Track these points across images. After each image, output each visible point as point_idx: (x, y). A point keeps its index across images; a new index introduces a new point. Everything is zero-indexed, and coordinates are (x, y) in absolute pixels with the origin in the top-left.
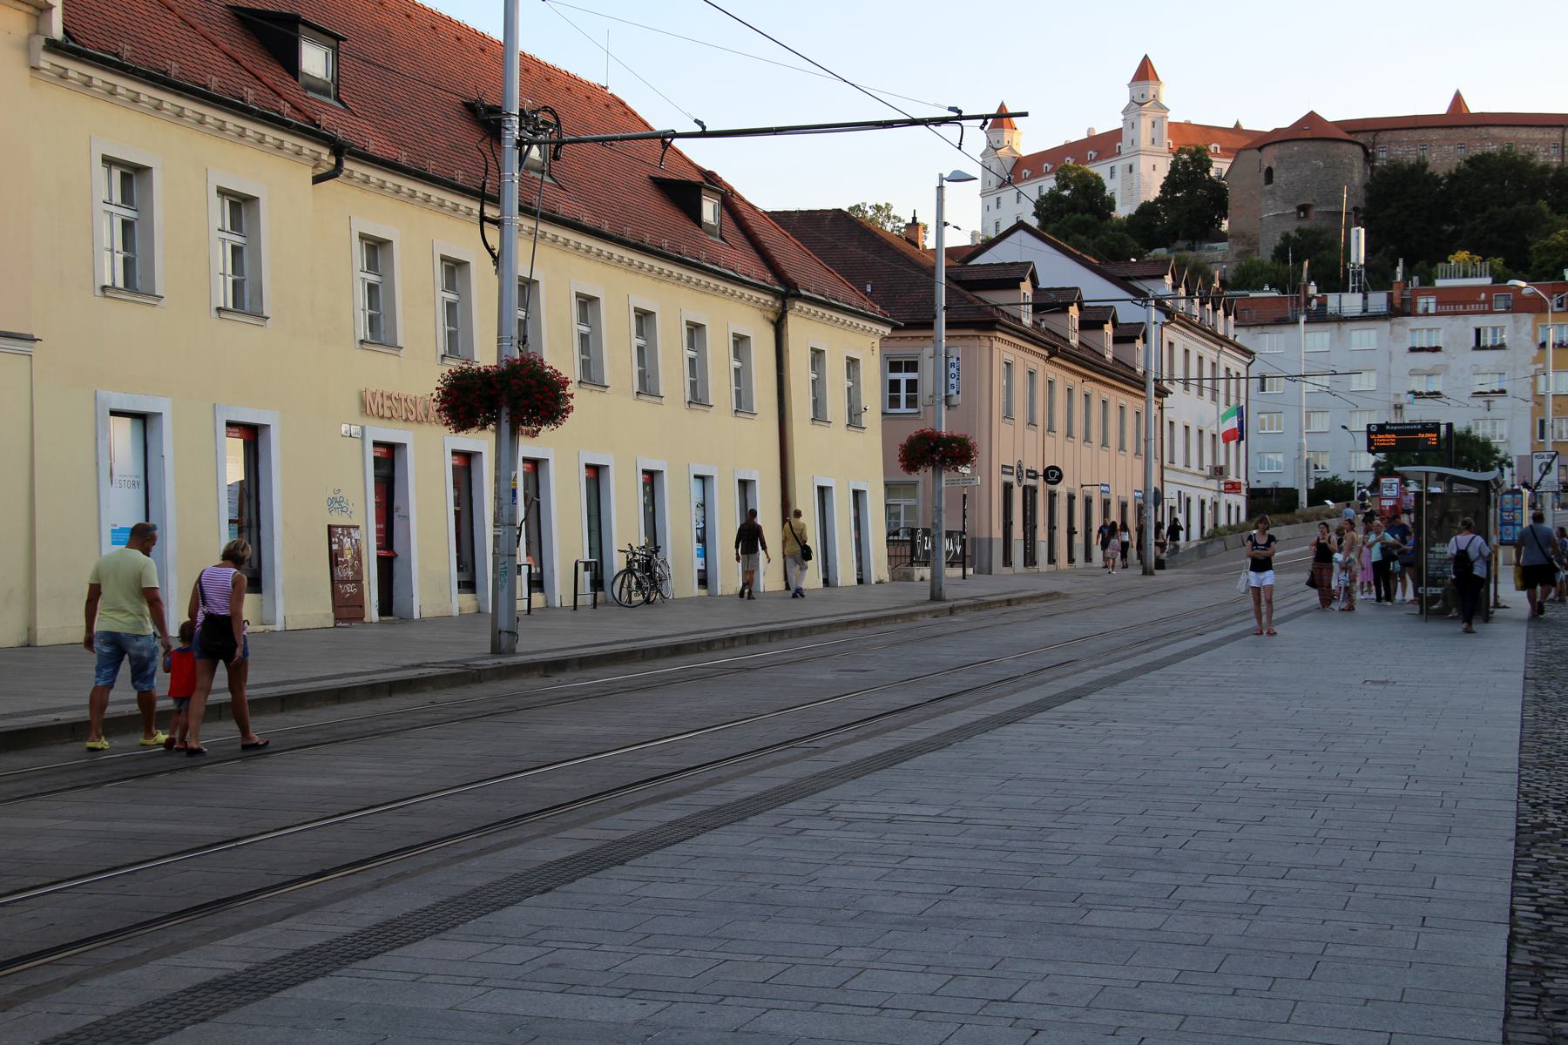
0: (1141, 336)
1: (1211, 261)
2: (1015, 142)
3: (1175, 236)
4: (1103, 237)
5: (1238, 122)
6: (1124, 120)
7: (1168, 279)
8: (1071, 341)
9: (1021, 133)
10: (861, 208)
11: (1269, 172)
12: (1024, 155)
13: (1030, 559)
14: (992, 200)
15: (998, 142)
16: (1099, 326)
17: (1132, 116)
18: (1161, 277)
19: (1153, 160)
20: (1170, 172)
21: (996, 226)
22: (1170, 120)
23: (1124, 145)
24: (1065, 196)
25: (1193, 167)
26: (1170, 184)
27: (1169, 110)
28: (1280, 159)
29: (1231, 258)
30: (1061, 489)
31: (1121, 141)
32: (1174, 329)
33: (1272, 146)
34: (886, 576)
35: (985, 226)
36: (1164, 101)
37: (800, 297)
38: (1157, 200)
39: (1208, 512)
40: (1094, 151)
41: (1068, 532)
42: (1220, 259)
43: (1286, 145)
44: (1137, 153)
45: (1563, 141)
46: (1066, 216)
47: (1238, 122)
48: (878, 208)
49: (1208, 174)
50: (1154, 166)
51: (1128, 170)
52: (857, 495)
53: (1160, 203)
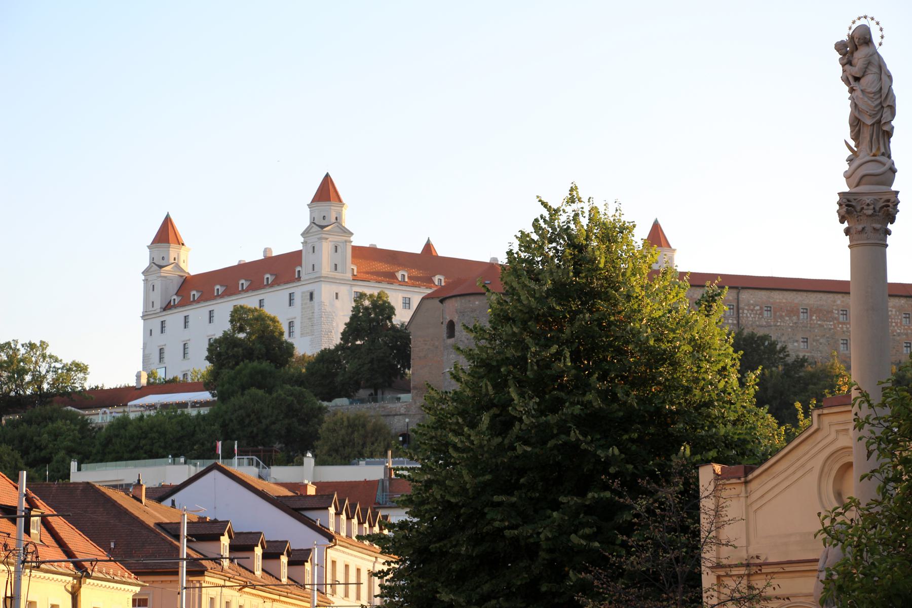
0: (309, 560)
1: (393, 413)
2: (182, 258)
3: (357, 387)
4: (280, 392)
5: (429, 240)
6: (304, 243)
7: (332, 510)
8: (256, 573)
9: (189, 249)
10: (13, 346)
11: (451, 326)
12: (192, 273)
14: (156, 324)
15: (163, 258)
16: (277, 556)
17: (312, 239)
18: (326, 508)
19: (334, 288)
20: (351, 318)
21: (160, 353)
22: (353, 244)
23: (304, 270)
24: (240, 339)
25: (376, 314)
26: (353, 329)
27: (352, 234)
28: (462, 313)
29: (413, 410)
31: (301, 265)
32: (337, 550)
33: (454, 299)
35: (147, 352)
36: (348, 224)
37: (89, 576)
38: (338, 347)
40: (271, 275)
42: (403, 411)
43: (468, 298)
44: (319, 279)
45: (738, 302)
46: (241, 364)
47: (429, 240)
48: (32, 346)
49: (391, 322)
50: (337, 294)
51: (309, 297)
53: (341, 350)
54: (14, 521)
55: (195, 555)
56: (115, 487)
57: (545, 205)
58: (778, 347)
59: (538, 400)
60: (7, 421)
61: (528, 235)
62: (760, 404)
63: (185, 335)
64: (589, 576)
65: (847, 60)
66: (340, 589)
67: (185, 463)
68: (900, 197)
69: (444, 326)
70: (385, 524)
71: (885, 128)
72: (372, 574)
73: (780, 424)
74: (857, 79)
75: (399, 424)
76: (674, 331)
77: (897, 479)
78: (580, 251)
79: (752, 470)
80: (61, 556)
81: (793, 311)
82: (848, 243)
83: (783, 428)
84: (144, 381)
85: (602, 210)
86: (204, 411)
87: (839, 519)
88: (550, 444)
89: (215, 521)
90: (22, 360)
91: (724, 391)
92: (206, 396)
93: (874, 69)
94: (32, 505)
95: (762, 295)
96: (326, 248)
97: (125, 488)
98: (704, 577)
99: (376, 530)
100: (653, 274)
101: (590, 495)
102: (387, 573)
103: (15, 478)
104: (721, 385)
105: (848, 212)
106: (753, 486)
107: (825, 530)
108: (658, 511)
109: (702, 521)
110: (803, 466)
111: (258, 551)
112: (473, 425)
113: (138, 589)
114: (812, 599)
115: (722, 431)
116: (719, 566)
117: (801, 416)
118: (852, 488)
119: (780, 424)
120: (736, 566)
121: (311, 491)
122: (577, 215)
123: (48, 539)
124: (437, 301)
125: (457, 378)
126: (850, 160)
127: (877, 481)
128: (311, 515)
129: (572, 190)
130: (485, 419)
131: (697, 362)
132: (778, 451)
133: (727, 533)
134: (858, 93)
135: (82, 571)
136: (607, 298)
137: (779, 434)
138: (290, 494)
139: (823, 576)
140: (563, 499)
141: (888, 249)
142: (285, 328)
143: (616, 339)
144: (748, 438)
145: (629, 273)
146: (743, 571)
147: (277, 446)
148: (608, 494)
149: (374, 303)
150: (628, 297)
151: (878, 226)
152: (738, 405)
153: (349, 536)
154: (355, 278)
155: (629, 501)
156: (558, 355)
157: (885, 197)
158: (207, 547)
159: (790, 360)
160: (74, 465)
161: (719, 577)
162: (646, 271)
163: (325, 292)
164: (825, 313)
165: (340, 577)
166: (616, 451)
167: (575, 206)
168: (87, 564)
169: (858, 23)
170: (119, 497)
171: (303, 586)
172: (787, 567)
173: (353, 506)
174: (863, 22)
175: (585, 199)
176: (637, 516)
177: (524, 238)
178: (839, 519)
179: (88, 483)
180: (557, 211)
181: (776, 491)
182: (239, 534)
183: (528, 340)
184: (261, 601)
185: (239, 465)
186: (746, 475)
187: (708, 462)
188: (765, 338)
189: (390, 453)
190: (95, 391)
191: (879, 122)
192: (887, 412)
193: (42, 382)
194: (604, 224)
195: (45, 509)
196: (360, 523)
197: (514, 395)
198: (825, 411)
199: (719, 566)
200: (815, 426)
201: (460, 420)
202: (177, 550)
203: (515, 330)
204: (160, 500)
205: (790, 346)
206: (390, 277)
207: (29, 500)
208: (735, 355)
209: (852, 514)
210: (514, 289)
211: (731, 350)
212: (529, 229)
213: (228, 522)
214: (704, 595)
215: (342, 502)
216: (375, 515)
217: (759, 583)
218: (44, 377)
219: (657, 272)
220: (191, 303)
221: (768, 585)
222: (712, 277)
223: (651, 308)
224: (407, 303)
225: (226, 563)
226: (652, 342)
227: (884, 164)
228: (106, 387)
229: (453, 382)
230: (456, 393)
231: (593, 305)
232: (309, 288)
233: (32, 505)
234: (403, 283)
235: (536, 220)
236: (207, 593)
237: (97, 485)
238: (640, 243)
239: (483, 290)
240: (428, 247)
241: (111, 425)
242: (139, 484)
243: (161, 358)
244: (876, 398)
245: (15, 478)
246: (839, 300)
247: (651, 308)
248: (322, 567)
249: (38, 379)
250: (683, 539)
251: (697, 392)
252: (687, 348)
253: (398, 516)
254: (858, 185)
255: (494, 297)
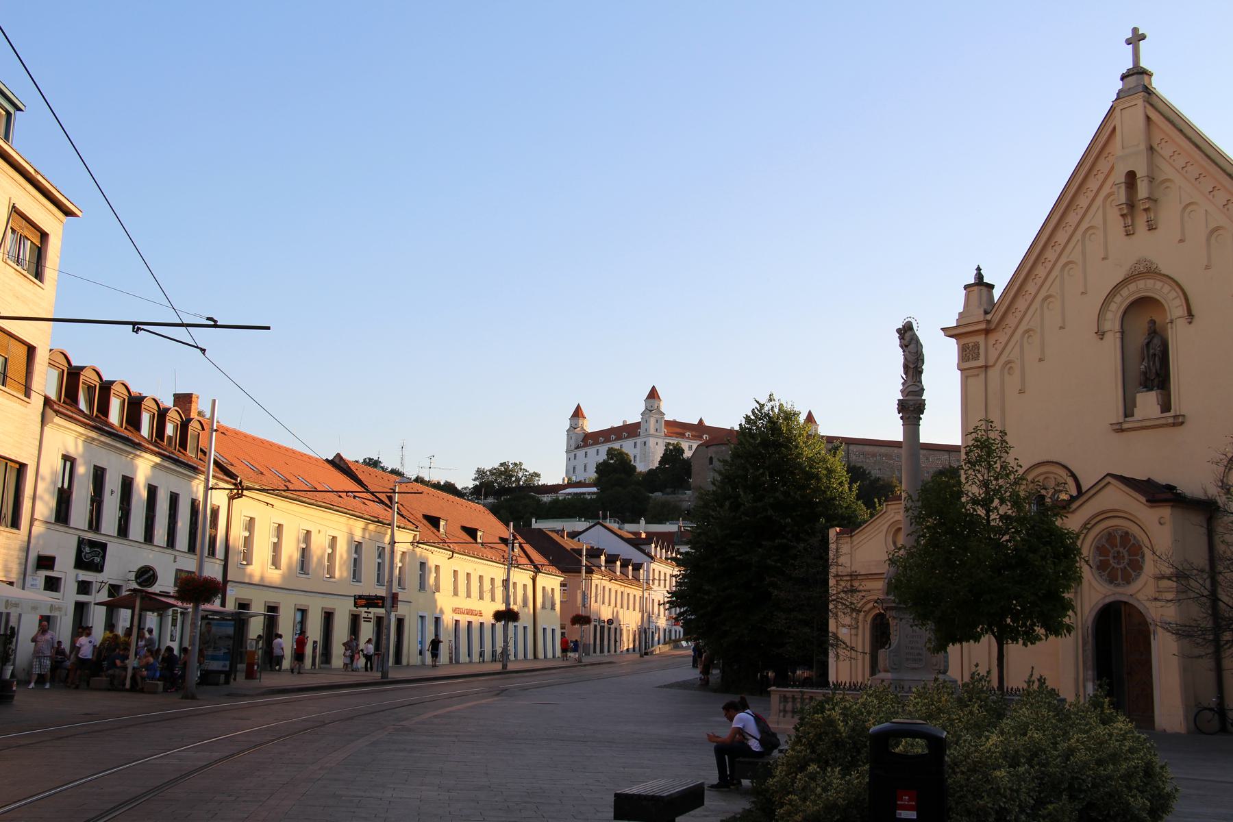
6: (642, 418)
7: (653, 545)
11: (711, 459)
13: (602, 651)
19: (656, 440)
23: (642, 431)
26: (664, 460)
27: (664, 414)
30: (613, 626)
34: (560, 656)
36: (663, 409)
37: (540, 572)
38: (657, 468)
39: (667, 633)
41: (216, 327)
42: (687, 499)
44: (649, 436)
48: (515, 464)
52: (553, 630)
54: (507, 546)
55: (589, 564)
56: (552, 531)
57: (758, 402)
58: (867, 472)
59: (752, 495)
60: (504, 499)
61: (749, 417)
62: (858, 499)
63: (586, 461)
64: (775, 579)
65: (902, 337)
66: (656, 582)
67: (585, 521)
68: (926, 402)
69: (708, 459)
70: (678, 552)
71: (920, 370)
72: (672, 576)
73: (867, 509)
74: (906, 346)
75: (687, 505)
76: (818, 464)
77: (924, 536)
78: (774, 425)
79: (854, 531)
80: (528, 562)
81: (874, 455)
82: (902, 423)
83: (869, 511)
84: (566, 482)
85: (785, 405)
86: (594, 497)
87: (896, 555)
88: (758, 516)
89: (598, 549)
90: (511, 471)
91: (842, 492)
92: (594, 490)
93: (914, 342)
94: (515, 538)
95: (860, 447)
96: (652, 421)
97: (557, 532)
98: (830, 581)
99: (674, 555)
100: (809, 436)
101: (777, 541)
102: (679, 576)
103: (507, 525)
104: (840, 490)
105: (902, 409)
106: (854, 538)
107: (890, 559)
108: (809, 549)
109: (830, 554)
110: (878, 529)
111: (618, 563)
112: (721, 506)
113: (562, 579)
114: (880, 591)
115: (840, 512)
116: (837, 575)
117: (877, 505)
118: (901, 540)
119: (867, 509)
120: (846, 576)
121: (643, 536)
122: (773, 407)
123: (522, 554)
124: (704, 447)
125: (713, 483)
126: (903, 384)
127: (915, 537)
128: (643, 547)
129: (770, 395)
130: (727, 503)
131: (829, 478)
132: (866, 522)
133: (841, 560)
134: (907, 353)
135: (537, 569)
136: (787, 447)
137: (867, 514)
138: (634, 537)
139: (886, 581)
140: (764, 543)
141: (920, 427)
142: (632, 459)
143: (791, 467)
144: (853, 515)
145: (797, 436)
146: (848, 578)
147: (628, 514)
148: (785, 541)
149: (674, 447)
150: (797, 447)
151: (915, 416)
152: (848, 500)
153: (661, 557)
154: (666, 435)
155: (795, 544)
156: (763, 474)
157: (919, 402)
158: (594, 561)
159: (872, 478)
160: (534, 520)
161: (837, 581)
162: (805, 435)
163: (652, 442)
164: (889, 456)
165: (657, 577)
166: (790, 521)
167: (772, 403)
168: (539, 566)
169: (907, 320)
170: (554, 536)
171: (639, 581)
172: (870, 576)
173: (663, 544)
174: (909, 319)
175: (777, 400)
176: (799, 551)
177: (747, 418)
178: (896, 555)
179: (540, 529)
180: (763, 405)
181: (865, 540)
182: (609, 555)
183: (748, 466)
184: (619, 586)
185: (610, 522)
186: (851, 533)
187: (833, 526)
188: (861, 467)
189: (681, 519)
190: (544, 486)
191: (917, 366)
192: (919, 504)
193: (520, 481)
194: (786, 412)
195: (521, 540)
196: (666, 552)
197: (741, 493)
198: (889, 503)
199: (837, 575)
200: (884, 510)
201: (715, 504)
202: (581, 561)
203: (743, 462)
204: (573, 538)
205: (872, 472)
206: (682, 435)
207: (514, 536)
208: (847, 476)
209: (902, 552)
210: (741, 441)
211: (845, 473)
212: (750, 414)
213: (604, 549)
214: (830, 589)
215: (658, 542)
216: (673, 548)
217: (856, 584)
218: (521, 479)
219: (811, 435)
220: (588, 446)
221: (860, 585)
222: (837, 438)
223: (808, 453)
224: (690, 448)
225: (603, 568)
226: (807, 469)
227: (918, 386)
228: (549, 484)
229: (712, 486)
230: (713, 491)
231: (780, 451)
232: (644, 440)
233: (515, 538)
234: (688, 438)
235: (753, 409)
236: (594, 582)
237: (544, 530)
238: (803, 421)
239: (727, 442)
240: (701, 421)
241: (551, 502)
242: (563, 530)
243: (574, 472)
244: (915, 497)
245: (507, 525)
246: (896, 450)
247: (808, 453)
248: (648, 571)
249: (518, 480)
250: (821, 562)
251: (829, 493)
252: (825, 472)
253: (684, 549)
254: (907, 396)
255: (732, 446)
